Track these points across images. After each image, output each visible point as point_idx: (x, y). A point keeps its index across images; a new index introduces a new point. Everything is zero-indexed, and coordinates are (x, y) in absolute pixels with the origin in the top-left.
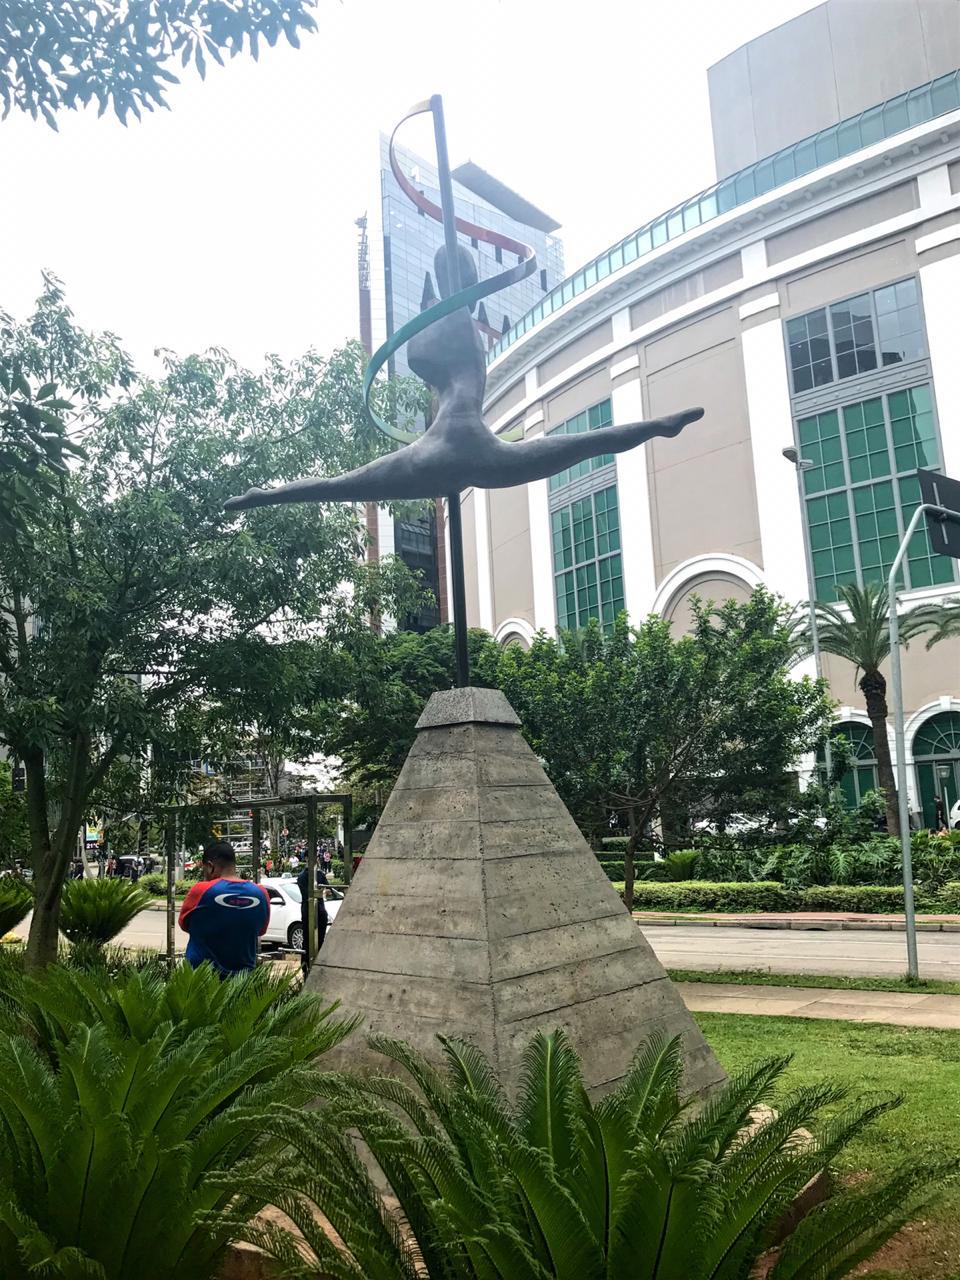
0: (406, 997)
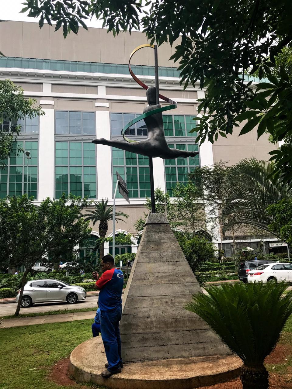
0: (173, 301)
